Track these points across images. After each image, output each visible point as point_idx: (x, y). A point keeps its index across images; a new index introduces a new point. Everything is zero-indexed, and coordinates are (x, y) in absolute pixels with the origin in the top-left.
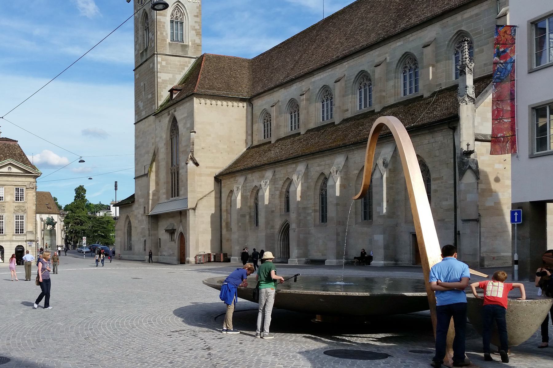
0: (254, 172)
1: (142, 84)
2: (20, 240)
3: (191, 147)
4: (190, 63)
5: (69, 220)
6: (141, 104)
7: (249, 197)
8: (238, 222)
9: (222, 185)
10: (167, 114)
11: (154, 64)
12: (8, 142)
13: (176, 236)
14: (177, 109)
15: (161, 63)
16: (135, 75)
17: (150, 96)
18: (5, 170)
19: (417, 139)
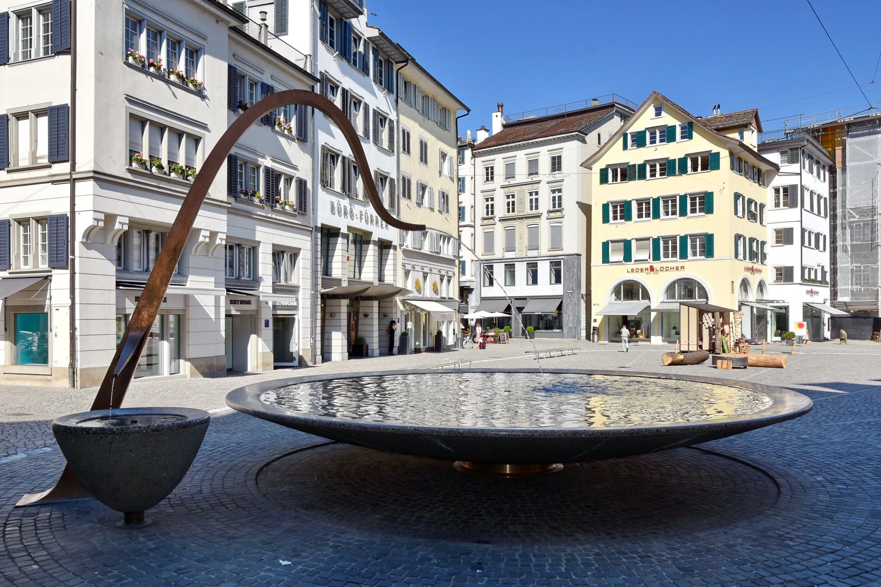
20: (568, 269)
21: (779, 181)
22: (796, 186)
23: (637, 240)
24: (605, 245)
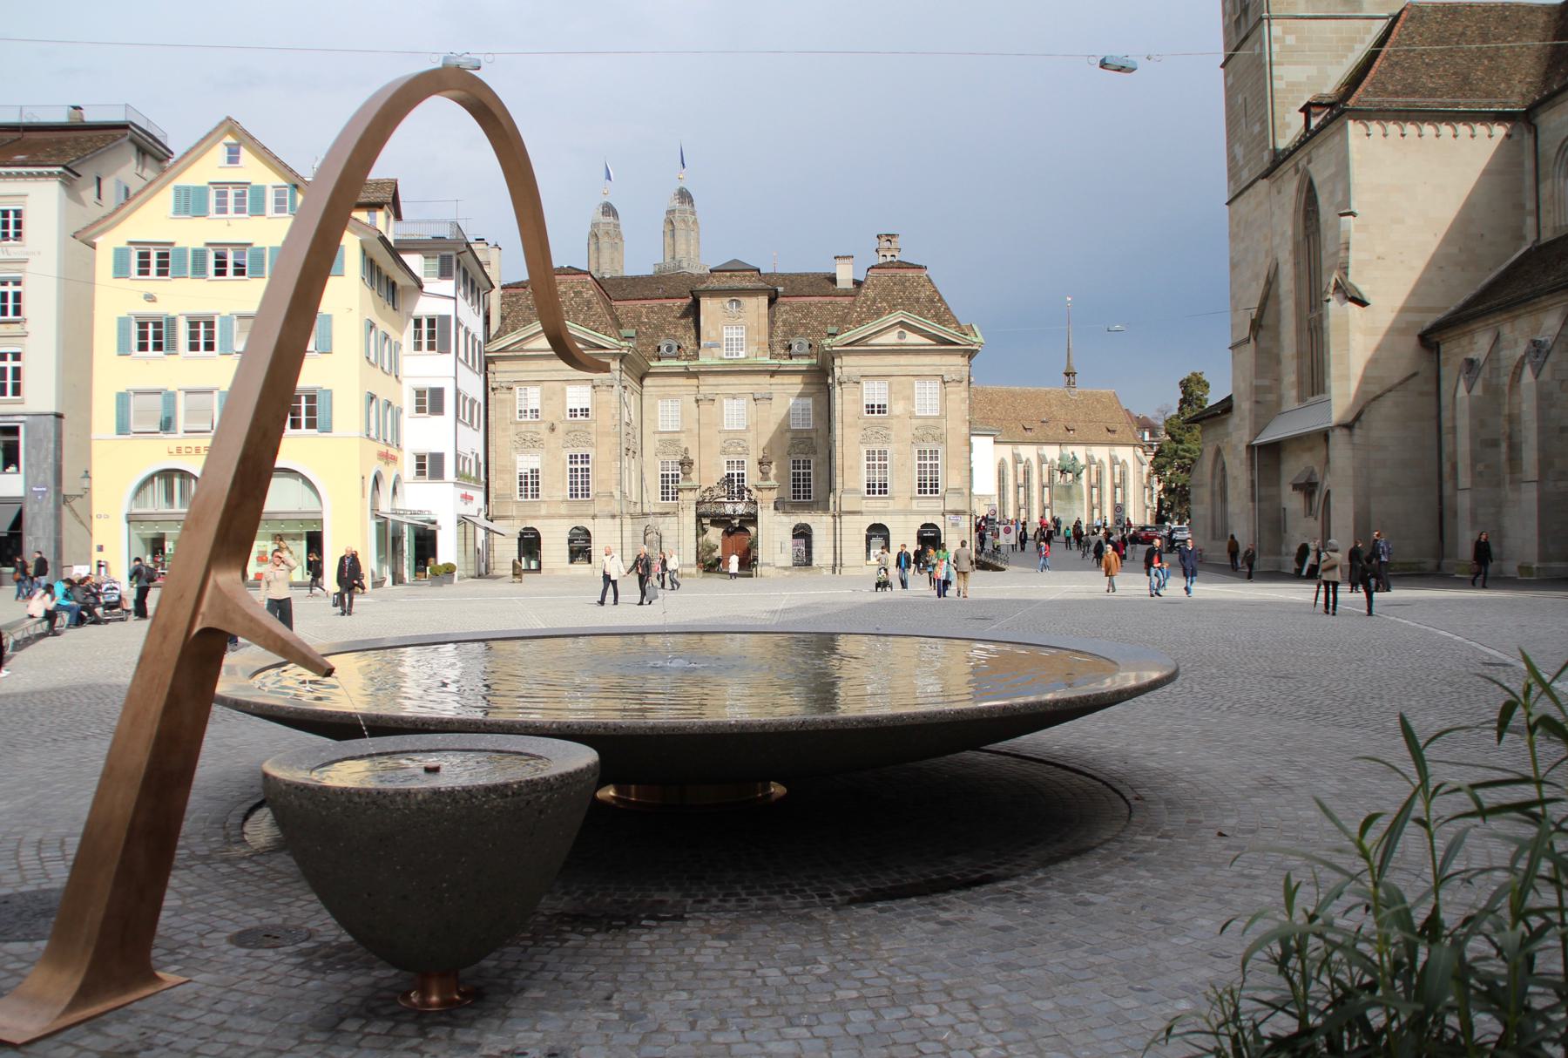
0: (1517, 317)
1: (1240, 99)
2: (929, 511)
3: (1342, 254)
4: (1368, 31)
5: (1162, 460)
6: (1239, 151)
7: (1506, 389)
8: (1475, 460)
9: (1442, 357)
10: (1292, 172)
11: (1262, 45)
12: (901, 272)
13: (1318, 499)
14: (1314, 155)
15: (1281, 40)
16: (1226, 77)
17: (1257, 128)
18: (891, 338)
19: (1541, 20)
20: (34, 443)
21: (425, 307)
22: (448, 318)
23: (188, 392)
24: (123, 400)
